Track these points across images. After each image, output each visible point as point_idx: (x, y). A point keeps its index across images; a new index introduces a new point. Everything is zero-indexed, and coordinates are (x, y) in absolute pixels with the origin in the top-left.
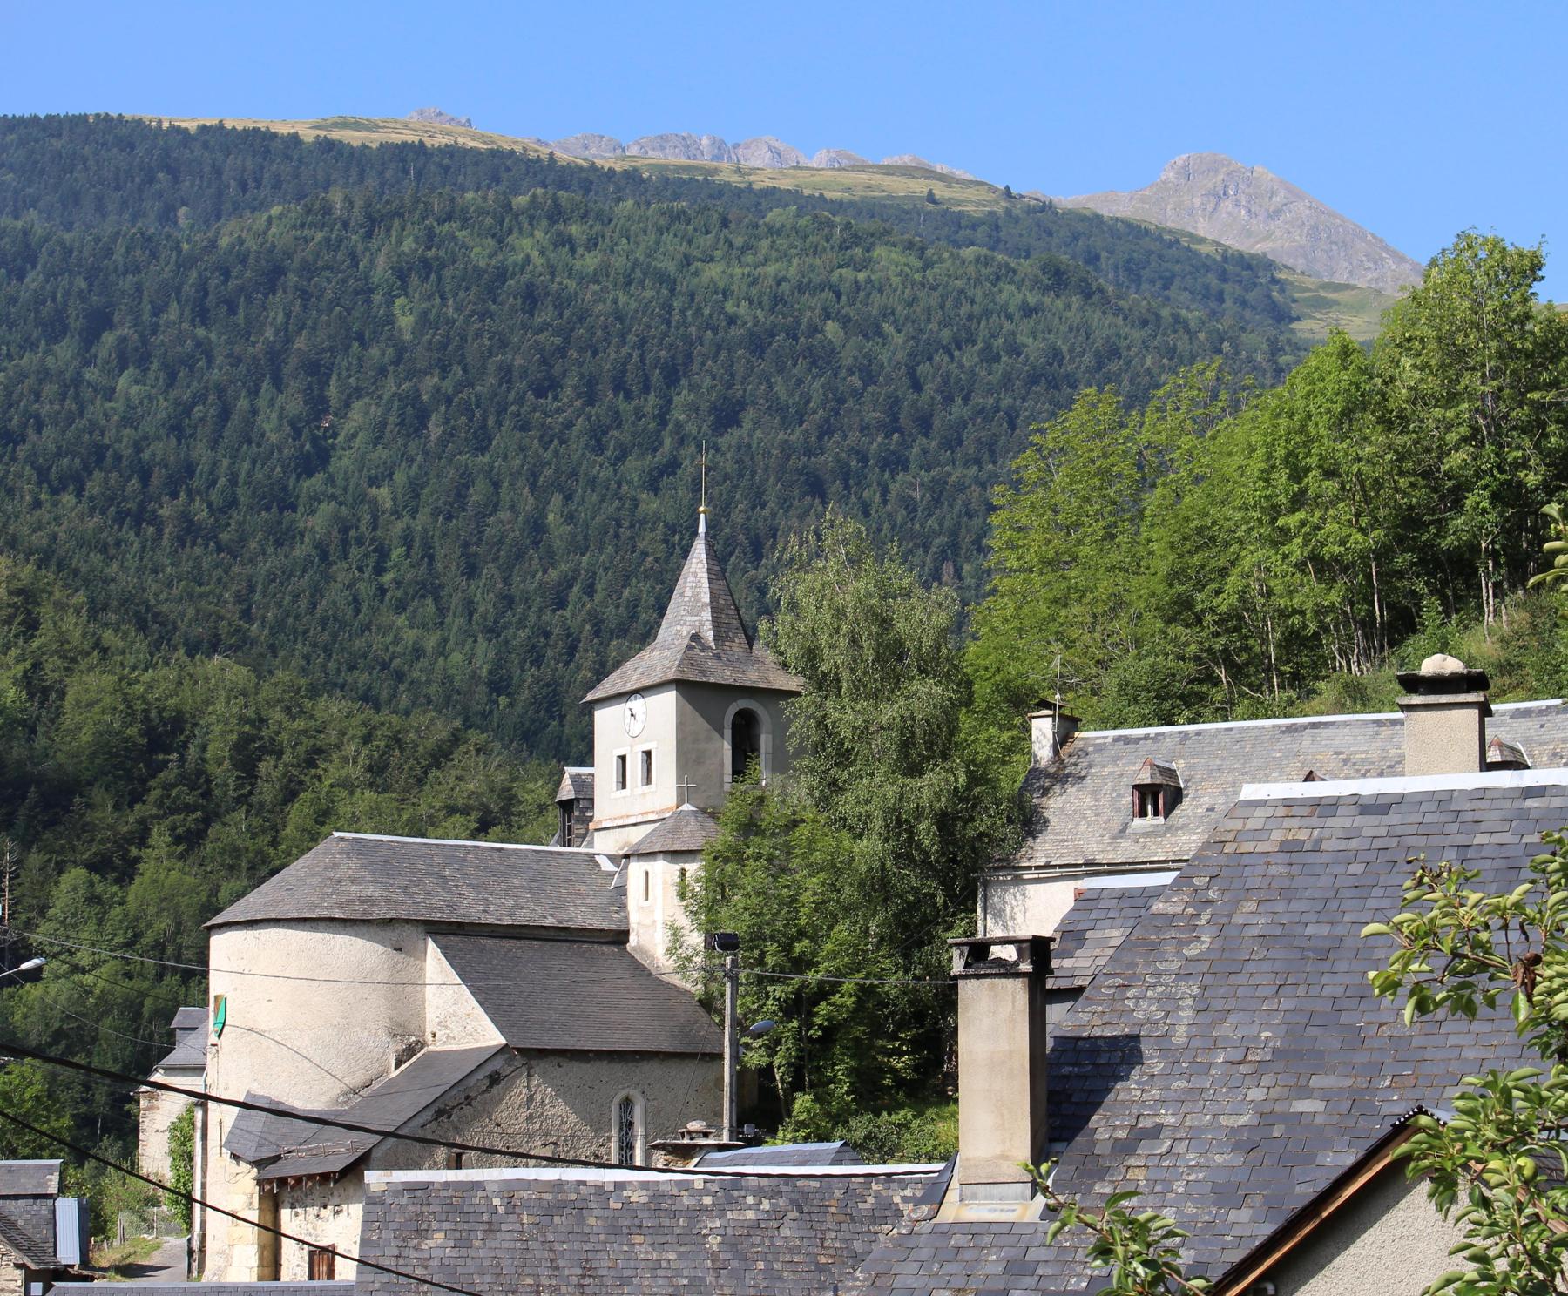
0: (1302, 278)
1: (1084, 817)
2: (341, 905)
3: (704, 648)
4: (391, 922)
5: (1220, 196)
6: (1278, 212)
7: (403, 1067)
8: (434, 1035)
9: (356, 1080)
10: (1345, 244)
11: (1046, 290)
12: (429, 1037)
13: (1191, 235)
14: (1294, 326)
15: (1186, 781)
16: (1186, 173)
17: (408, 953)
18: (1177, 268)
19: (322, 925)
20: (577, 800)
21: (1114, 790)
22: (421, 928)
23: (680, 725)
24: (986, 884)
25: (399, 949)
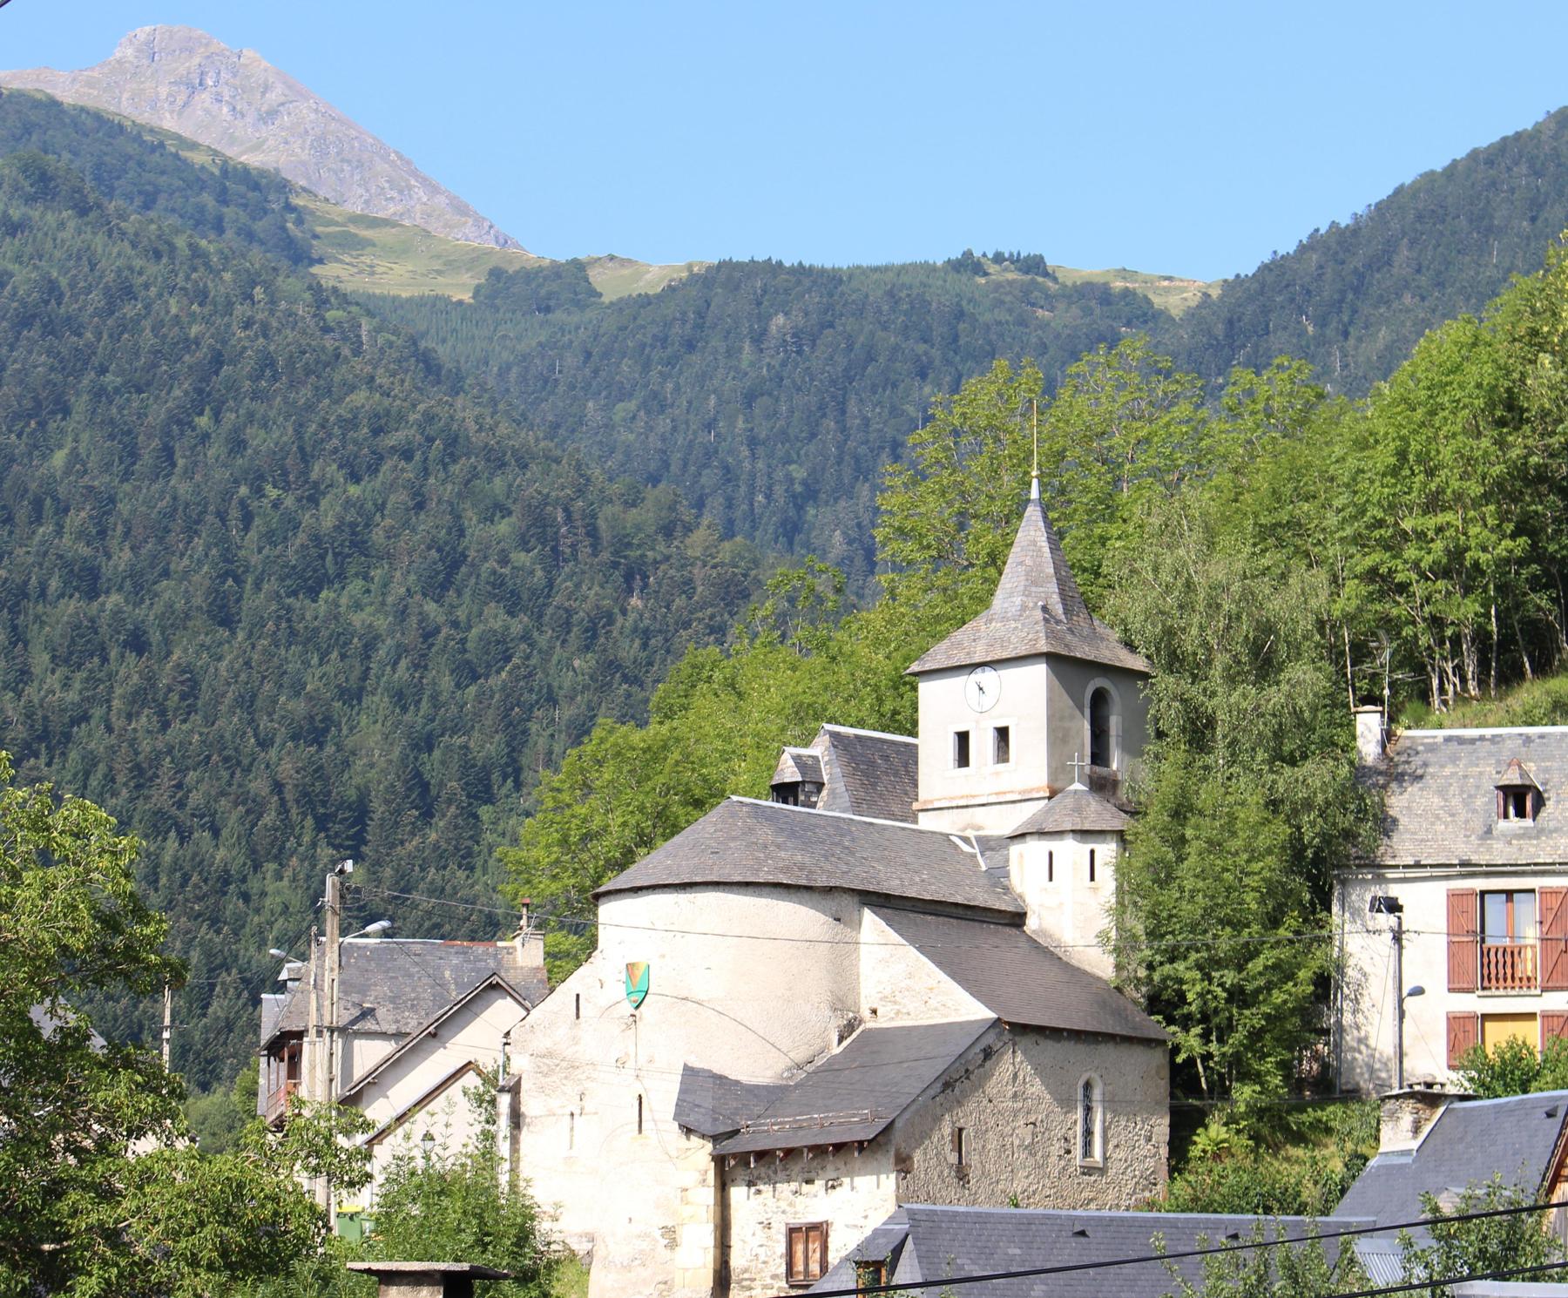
0: (328, 207)
1: (1438, 817)
2: (782, 870)
3: (1058, 622)
4: (829, 890)
5: (194, 86)
6: (272, 114)
7: (849, 1040)
8: (874, 1012)
9: (800, 1055)
10: (360, 164)
11: (30, 200)
12: (866, 1014)
13: (179, 137)
14: (316, 269)
15: (1542, 784)
16: (150, 52)
17: (845, 924)
18: (163, 180)
19: (767, 890)
20: (803, 782)
21: (1462, 792)
22: (856, 899)
23: (1050, 701)
24: (1344, 883)
25: (838, 920)
